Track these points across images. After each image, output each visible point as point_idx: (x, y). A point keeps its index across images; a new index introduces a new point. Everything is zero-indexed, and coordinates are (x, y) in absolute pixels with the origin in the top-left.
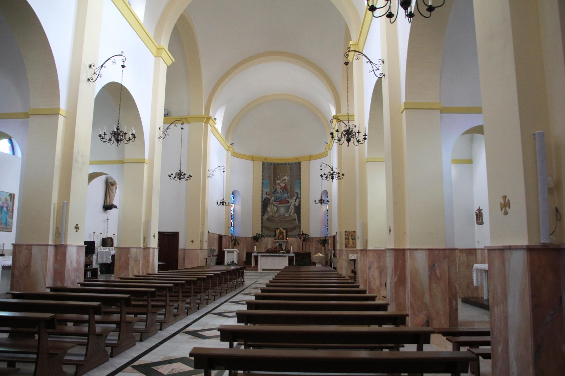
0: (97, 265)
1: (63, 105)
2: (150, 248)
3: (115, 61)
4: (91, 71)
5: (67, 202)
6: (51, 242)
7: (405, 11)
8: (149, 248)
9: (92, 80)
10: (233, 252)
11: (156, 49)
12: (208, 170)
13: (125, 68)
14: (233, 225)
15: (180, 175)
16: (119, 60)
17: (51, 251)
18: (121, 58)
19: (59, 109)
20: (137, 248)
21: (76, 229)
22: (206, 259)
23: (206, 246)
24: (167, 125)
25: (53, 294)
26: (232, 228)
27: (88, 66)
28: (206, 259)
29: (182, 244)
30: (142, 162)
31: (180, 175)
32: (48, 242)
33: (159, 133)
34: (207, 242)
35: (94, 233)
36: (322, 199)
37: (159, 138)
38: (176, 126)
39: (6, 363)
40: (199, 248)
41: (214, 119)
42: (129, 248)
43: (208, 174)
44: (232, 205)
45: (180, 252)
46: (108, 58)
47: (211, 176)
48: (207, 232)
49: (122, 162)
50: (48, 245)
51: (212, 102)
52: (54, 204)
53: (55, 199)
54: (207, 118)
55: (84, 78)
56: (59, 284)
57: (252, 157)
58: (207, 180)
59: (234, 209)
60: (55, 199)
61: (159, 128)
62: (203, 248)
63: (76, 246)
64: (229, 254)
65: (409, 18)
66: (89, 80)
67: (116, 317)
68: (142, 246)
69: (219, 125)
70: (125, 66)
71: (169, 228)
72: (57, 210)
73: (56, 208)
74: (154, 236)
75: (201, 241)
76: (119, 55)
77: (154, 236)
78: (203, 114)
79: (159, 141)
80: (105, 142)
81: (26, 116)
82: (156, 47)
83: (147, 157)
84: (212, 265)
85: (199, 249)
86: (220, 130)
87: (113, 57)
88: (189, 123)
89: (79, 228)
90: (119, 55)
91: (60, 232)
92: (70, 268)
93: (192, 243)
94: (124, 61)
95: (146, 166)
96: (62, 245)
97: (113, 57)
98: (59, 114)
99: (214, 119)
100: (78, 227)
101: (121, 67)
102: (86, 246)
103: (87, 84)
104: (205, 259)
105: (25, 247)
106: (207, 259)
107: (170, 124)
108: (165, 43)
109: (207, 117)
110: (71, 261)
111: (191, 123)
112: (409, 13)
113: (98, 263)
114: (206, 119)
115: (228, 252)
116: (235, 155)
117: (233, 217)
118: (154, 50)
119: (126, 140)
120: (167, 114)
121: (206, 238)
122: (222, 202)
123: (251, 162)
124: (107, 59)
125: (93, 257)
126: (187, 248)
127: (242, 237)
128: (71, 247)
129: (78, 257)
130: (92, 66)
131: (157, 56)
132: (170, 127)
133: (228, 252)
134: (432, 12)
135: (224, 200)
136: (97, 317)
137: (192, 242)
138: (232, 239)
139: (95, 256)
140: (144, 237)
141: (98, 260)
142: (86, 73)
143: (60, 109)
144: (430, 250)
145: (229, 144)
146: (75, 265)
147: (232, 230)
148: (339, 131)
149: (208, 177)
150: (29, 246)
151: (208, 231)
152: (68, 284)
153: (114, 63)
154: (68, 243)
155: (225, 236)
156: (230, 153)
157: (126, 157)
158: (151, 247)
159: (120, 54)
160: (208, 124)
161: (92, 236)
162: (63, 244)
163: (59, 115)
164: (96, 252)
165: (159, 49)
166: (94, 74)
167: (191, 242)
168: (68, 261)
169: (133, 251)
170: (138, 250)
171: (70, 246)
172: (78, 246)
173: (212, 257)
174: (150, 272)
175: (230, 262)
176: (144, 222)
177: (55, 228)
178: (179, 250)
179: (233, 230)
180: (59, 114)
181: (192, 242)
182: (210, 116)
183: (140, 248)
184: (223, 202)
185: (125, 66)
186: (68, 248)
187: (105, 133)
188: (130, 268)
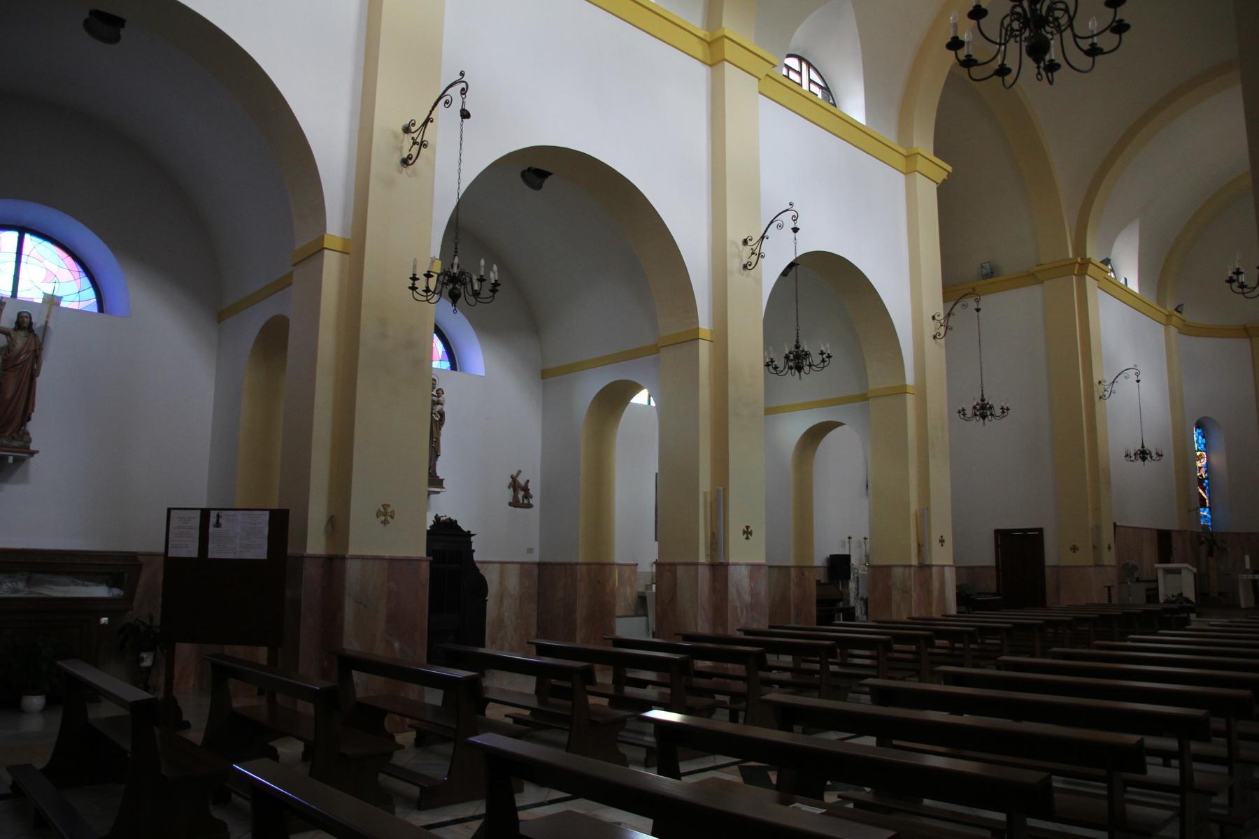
0: (859, 601)
1: (704, 321)
2: (932, 566)
3: (781, 222)
4: (748, 249)
5: (724, 489)
6: (702, 558)
7: (1036, 65)
8: (930, 566)
9: (750, 265)
10: (1178, 571)
11: (903, 157)
12: (1100, 382)
13: (799, 231)
14: (1210, 503)
15: (983, 410)
16: (786, 218)
17: (704, 575)
18: (791, 214)
19: (697, 329)
20: (904, 566)
21: (745, 535)
22: (1109, 588)
23: (1109, 558)
24: (950, 304)
25: (711, 648)
26: (1205, 512)
27: (740, 243)
28: (1109, 588)
29: (1053, 554)
30: (901, 391)
31: (983, 410)
32: (698, 559)
33: (930, 328)
34: (1113, 550)
35: (850, 538)
36: (1145, 448)
37: (935, 337)
38: (964, 306)
39: (644, 750)
40: (1092, 563)
41: (1102, 262)
42: (889, 567)
43: (1098, 390)
44: (1200, 455)
45: (1048, 572)
46: (770, 220)
47: (1107, 394)
48: (1112, 525)
49: (864, 398)
50: (697, 564)
51: (1089, 223)
52: (705, 493)
53: (705, 484)
54: (1080, 264)
55: (734, 265)
56: (720, 632)
57: (1245, 329)
58: (1098, 405)
59: (1207, 463)
60: (705, 484)
61: (931, 319)
62: (1101, 564)
63: (748, 565)
64: (1170, 576)
65: (1050, 74)
66: (745, 267)
67: (1218, 747)
68: (914, 561)
69: (1128, 274)
70: (798, 229)
71: (1017, 521)
72: (711, 507)
73: (709, 500)
74: (942, 541)
75: (1094, 547)
76: (787, 210)
77: (942, 541)
78: (1071, 255)
79: (936, 343)
80: (782, 374)
81: (655, 349)
82: (903, 155)
83: (910, 379)
84: (1131, 602)
85: (1090, 566)
86: (1134, 286)
87: (778, 215)
88: (1042, 282)
89: (742, 533)
90: (787, 210)
91: (717, 541)
92: (738, 603)
93: (1074, 552)
94: (795, 220)
95: (910, 400)
96: (721, 564)
97: (778, 215)
98: (699, 338)
99: (1102, 262)
100: (749, 530)
101: (791, 231)
102: (431, 558)
103: (742, 275)
104: (1106, 589)
105: (668, 567)
106: (1112, 589)
107: (953, 303)
108: (924, 144)
109: (1079, 260)
110: (737, 590)
111: (1045, 282)
112: (1047, 63)
113: (860, 596)
114: (1077, 266)
115: (1167, 571)
116: (1189, 330)
117: (1208, 484)
118: (901, 162)
119: (1075, 36)
120: (992, 273)
121: (1108, 536)
122: (978, 407)
123: (1244, 343)
124: (769, 223)
125: (848, 585)
126: (1062, 564)
127: (1251, 533)
128: (737, 566)
129: (752, 585)
130: (936, 317)
131: (909, 172)
132: (953, 311)
133: (1167, 571)
134: (1125, 35)
135: (986, 402)
136: (1195, 747)
137: (1074, 549)
138: (1203, 539)
139: (852, 585)
140: (919, 545)
141: (860, 591)
142: (737, 255)
143: (700, 331)
144: (522, 564)
145: (1170, 308)
146: (747, 598)
147: (1205, 516)
148: (831, 357)
149: (1100, 398)
150: (673, 565)
151: (1115, 524)
152: (733, 631)
153: (780, 226)
154: (731, 560)
155: (1179, 532)
156: (1173, 330)
157: (871, 387)
158: (934, 563)
159: (789, 207)
160: (1087, 277)
161: (863, 546)
162: (723, 561)
163: (700, 340)
164: (856, 575)
165: (910, 157)
166: (753, 254)
167: (1071, 549)
168: (732, 590)
169: (897, 572)
170: (907, 570)
171: (735, 564)
172: (753, 565)
173: (1129, 584)
174: (935, 614)
175: (1173, 596)
176: (916, 514)
177: (709, 535)
178: (1046, 569)
179: (1209, 516)
180: (699, 338)
181: (1074, 549)
182: (1088, 256)
183: (910, 566)
184: (983, 407)
185: (798, 229)
186: (731, 568)
187: (772, 359)
188: (894, 608)
